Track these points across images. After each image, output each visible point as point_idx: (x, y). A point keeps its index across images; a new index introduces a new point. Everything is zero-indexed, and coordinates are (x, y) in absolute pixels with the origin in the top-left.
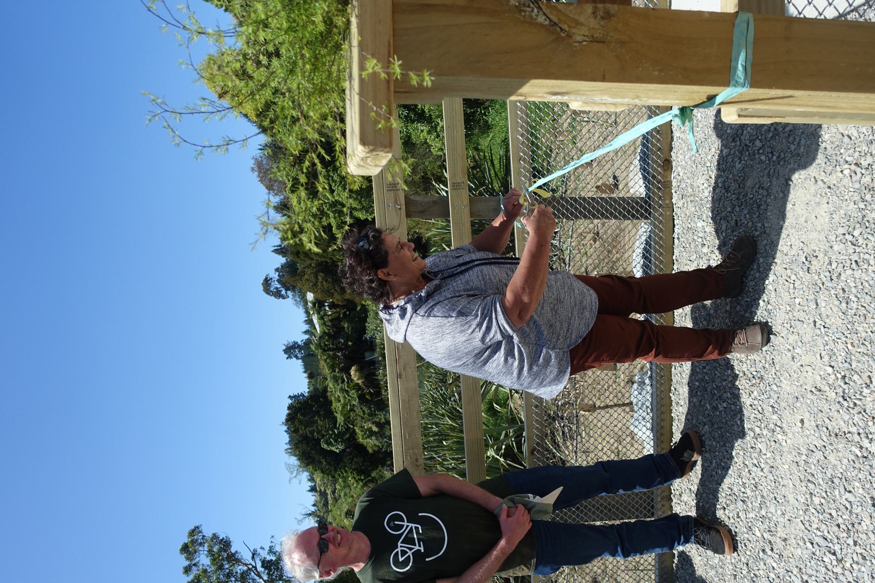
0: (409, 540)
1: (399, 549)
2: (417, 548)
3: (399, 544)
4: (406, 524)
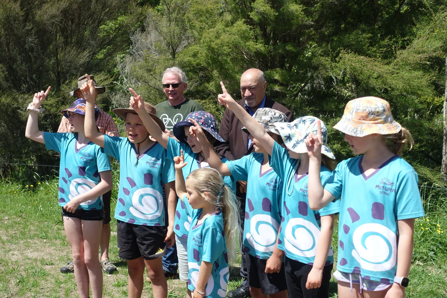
3: (170, 119)
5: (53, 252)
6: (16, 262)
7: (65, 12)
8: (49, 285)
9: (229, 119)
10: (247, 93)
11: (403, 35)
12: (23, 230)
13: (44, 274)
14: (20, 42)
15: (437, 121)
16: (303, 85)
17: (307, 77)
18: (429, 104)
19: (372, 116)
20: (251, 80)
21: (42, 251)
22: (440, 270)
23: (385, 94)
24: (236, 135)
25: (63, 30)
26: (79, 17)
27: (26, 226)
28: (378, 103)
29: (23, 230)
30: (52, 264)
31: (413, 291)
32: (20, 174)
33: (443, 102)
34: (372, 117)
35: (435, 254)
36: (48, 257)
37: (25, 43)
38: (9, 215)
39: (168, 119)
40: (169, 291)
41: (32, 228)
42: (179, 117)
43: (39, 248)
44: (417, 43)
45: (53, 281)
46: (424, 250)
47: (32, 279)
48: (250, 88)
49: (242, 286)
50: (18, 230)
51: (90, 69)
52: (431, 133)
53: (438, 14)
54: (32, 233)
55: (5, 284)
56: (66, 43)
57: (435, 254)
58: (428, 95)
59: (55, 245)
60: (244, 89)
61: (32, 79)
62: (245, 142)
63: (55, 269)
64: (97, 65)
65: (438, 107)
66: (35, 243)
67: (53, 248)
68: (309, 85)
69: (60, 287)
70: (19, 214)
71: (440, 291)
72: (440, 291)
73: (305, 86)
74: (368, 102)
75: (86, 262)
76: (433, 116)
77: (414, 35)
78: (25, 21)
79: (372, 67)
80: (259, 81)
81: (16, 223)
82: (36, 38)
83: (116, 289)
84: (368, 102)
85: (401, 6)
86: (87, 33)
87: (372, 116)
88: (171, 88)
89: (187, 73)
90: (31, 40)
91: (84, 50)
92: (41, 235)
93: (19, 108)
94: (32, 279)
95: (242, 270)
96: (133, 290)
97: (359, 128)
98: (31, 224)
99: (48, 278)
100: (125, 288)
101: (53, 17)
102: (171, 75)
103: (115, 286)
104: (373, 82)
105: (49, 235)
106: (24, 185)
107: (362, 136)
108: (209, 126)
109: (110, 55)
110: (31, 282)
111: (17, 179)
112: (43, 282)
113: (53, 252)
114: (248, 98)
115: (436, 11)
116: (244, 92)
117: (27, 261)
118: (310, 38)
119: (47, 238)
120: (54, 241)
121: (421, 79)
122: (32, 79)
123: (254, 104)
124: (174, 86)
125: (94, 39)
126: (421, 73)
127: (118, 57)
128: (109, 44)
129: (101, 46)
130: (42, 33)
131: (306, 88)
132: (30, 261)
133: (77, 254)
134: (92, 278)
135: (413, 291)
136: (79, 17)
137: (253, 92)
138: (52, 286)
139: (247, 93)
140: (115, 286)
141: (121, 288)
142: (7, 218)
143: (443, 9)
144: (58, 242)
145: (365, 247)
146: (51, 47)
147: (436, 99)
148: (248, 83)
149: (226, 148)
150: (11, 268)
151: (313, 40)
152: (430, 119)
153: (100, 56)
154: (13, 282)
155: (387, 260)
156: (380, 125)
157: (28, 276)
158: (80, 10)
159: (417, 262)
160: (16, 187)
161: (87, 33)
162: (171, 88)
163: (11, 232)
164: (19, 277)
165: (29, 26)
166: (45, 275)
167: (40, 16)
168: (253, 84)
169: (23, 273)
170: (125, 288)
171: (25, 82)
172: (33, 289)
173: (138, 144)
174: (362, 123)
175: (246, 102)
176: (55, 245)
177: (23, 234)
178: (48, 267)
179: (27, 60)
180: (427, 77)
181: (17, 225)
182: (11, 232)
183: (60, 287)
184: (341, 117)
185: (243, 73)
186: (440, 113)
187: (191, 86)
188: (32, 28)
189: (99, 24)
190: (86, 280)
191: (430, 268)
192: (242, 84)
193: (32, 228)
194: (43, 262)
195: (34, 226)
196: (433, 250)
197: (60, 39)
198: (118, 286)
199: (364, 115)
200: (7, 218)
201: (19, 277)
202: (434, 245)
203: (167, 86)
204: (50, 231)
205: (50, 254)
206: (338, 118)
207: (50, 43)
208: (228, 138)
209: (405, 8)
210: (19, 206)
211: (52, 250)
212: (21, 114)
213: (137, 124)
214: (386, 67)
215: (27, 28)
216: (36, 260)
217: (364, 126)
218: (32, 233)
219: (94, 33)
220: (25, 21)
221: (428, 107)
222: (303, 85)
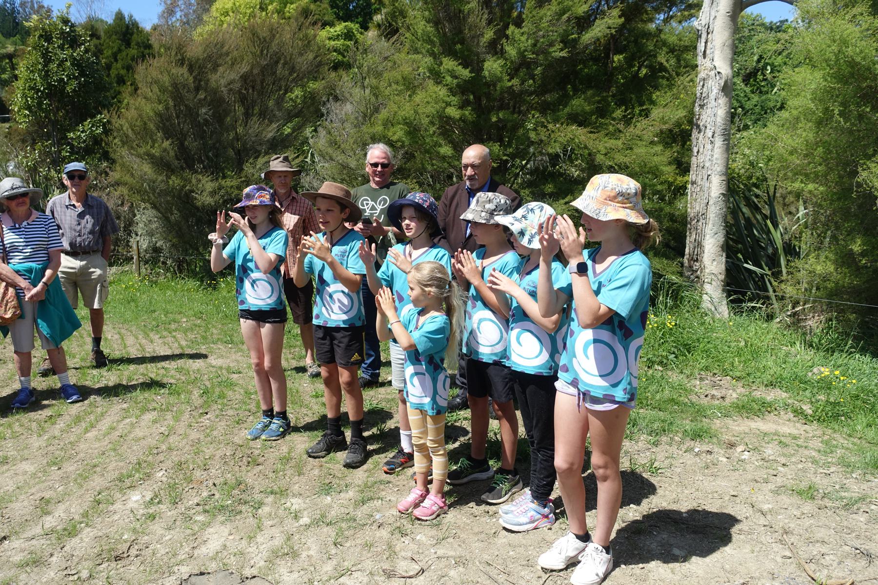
0: (373, 208)
1: (370, 202)
2: (368, 211)
4: (381, 207)
6: (198, 370)
7: (244, 78)
8: (237, 396)
10: (470, 172)
11: (641, 105)
12: (204, 334)
14: (191, 114)
15: (680, 205)
16: (524, 162)
17: (529, 153)
18: (670, 184)
19: (622, 198)
20: (475, 157)
21: (227, 358)
22: (682, 376)
24: (454, 220)
25: (243, 100)
26: (262, 83)
27: (207, 329)
28: (630, 185)
29: (204, 334)
30: (240, 373)
31: (651, 399)
32: (198, 269)
34: (620, 199)
35: (676, 357)
36: (235, 364)
37: (198, 115)
38: (187, 317)
39: (371, 203)
41: (215, 331)
43: (224, 354)
44: (656, 113)
45: (242, 391)
46: (664, 354)
47: (217, 390)
48: (473, 166)
49: (458, 396)
50: (198, 333)
51: (277, 145)
52: (672, 218)
54: (215, 337)
55: (188, 396)
56: (247, 115)
57: (676, 357)
58: (669, 172)
60: (466, 166)
61: (208, 157)
62: (464, 229)
63: (243, 378)
64: (283, 140)
65: (681, 188)
66: (219, 349)
67: (240, 354)
68: (532, 162)
70: (199, 315)
71: (682, 399)
72: (682, 399)
73: (526, 164)
74: (619, 180)
75: (266, 368)
76: (675, 198)
77: (653, 103)
78: (197, 89)
80: (484, 160)
81: (196, 326)
82: (210, 110)
83: (314, 400)
84: (619, 180)
85: (639, 69)
86: (271, 103)
87: (622, 198)
88: (379, 169)
91: (271, 122)
92: (225, 340)
93: (193, 191)
94: (217, 390)
95: (458, 376)
98: (213, 326)
99: (236, 388)
101: (231, 82)
102: (376, 153)
103: (312, 397)
105: (235, 339)
106: (202, 281)
107: (604, 220)
109: (298, 129)
112: (230, 393)
114: (471, 178)
116: (466, 170)
117: (211, 369)
118: (531, 107)
120: (240, 346)
122: (208, 157)
123: (477, 186)
124: (384, 166)
125: (280, 110)
127: (308, 131)
129: (289, 117)
130: (217, 102)
131: (529, 166)
132: (214, 370)
133: (256, 361)
134: (274, 386)
135: (651, 399)
136: (262, 83)
140: (312, 397)
141: (320, 399)
142: (185, 320)
145: (519, 343)
146: (229, 119)
147: (680, 179)
150: (193, 377)
151: (535, 109)
153: (287, 130)
154: (196, 393)
155: (537, 357)
156: (628, 210)
157: (213, 387)
158: (264, 75)
159: (656, 367)
160: (192, 284)
161: (271, 103)
162: (379, 169)
163: (191, 336)
165: (202, 95)
166: (231, 385)
167: (216, 81)
168: (477, 162)
169: (208, 383)
171: (201, 161)
172: (219, 401)
173: (331, 232)
174: (608, 205)
177: (204, 338)
178: (235, 376)
180: (668, 153)
182: (191, 336)
186: (684, 194)
187: (397, 163)
189: (286, 92)
190: (267, 389)
191: (670, 373)
193: (215, 331)
194: (228, 370)
196: (674, 353)
197: (239, 110)
198: (317, 397)
199: (613, 194)
200: (185, 320)
201: (202, 387)
202: (676, 347)
203: (375, 165)
204: (235, 335)
205: (238, 361)
207: (227, 115)
209: (644, 71)
210: (197, 307)
211: (238, 356)
212: (196, 199)
213: (329, 210)
215: (198, 97)
216: (221, 368)
217: (609, 209)
218: (215, 337)
219: (279, 102)
220: (197, 89)
221: (669, 188)
222: (524, 162)
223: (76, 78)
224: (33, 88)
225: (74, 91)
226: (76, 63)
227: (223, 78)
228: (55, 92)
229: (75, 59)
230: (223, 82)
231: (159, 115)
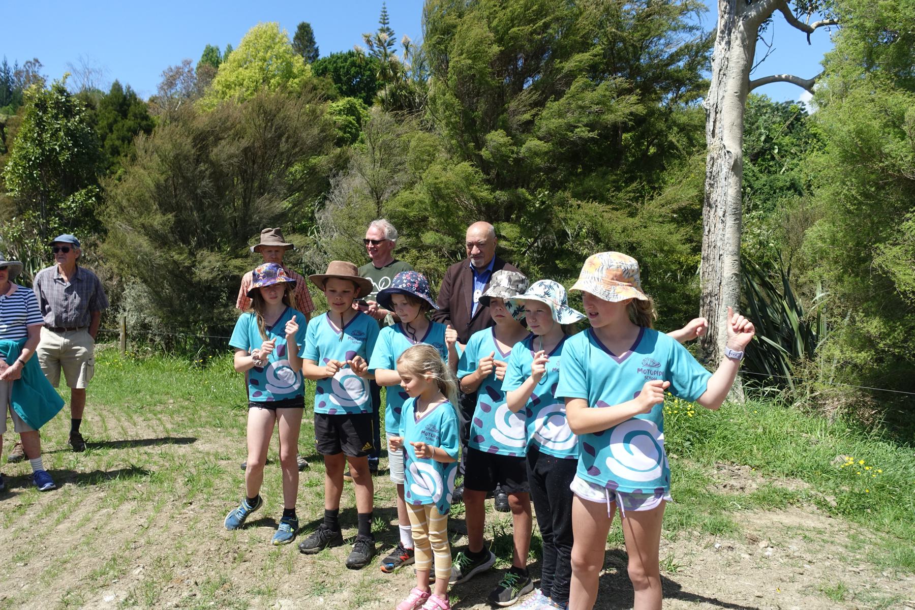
4: (382, 288)
5: (229, 443)
6: (184, 456)
7: (246, 150)
8: (225, 485)
9: (451, 282)
10: (475, 250)
12: (191, 416)
13: (219, 472)
19: (624, 277)
20: (480, 235)
21: (216, 443)
22: (699, 465)
23: (631, 250)
24: (458, 301)
25: (243, 173)
27: (195, 411)
29: (191, 416)
30: (229, 459)
33: (698, 262)
35: (691, 444)
36: (223, 449)
38: (174, 398)
40: (375, 491)
41: (203, 414)
42: (386, 281)
44: (669, 192)
45: (230, 479)
46: (679, 440)
48: (478, 244)
50: (185, 416)
53: (692, 158)
54: (203, 420)
55: (171, 484)
57: (691, 444)
59: (231, 435)
60: (471, 245)
65: (692, 267)
66: (207, 433)
69: (238, 488)
70: (187, 396)
71: (699, 489)
79: (616, 222)
80: (488, 236)
81: (183, 407)
83: (308, 490)
89: (399, 227)
90: (206, 184)
92: (214, 423)
94: (203, 478)
96: (331, 491)
97: (612, 291)
98: (202, 408)
100: (318, 489)
101: (231, 157)
102: (378, 229)
104: (616, 238)
105: (225, 423)
107: (616, 301)
108: (423, 292)
110: (203, 481)
111: (183, 353)
112: (217, 481)
113: (229, 443)
114: (476, 257)
115: (690, 154)
117: (198, 454)
119: (221, 426)
120: (230, 430)
121: (676, 237)
126: (673, 226)
128: (298, 190)
130: (218, 175)
132: (201, 455)
137: (483, 249)
138: (229, 486)
139: (475, 250)
141: (314, 488)
142: (172, 401)
143: (698, 151)
144: (235, 431)
148: (477, 239)
149: (445, 316)
150: (178, 464)
152: (684, 282)
154: (180, 481)
157: (199, 474)
160: (182, 363)
164: (187, 474)
165: (202, 167)
166: (219, 472)
168: (483, 240)
169: (193, 470)
170: (318, 489)
172: (205, 490)
175: (473, 261)
176: (231, 435)
177: (192, 421)
178: (224, 463)
179: (200, 208)
181: (185, 411)
183: (238, 488)
184: (577, 277)
185: (469, 226)
188: (206, 170)
192: (469, 239)
193: (203, 414)
194: (217, 456)
195: (205, 411)
196: (689, 440)
198: (311, 486)
200: (172, 401)
201: (187, 474)
202: (690, 433)
204: (225, 418)
205: (226, 446)
206: (573, 280)
208: (449, 304)
209: (652, 150)
211: (227, 441)
213: (345, 292)
214: (631, 220)
216: (208, 454)
217: (618, 289)
218: (203, 420)
220: (198, 161)
223: (69, 149)
224: (25, 157)
225: (67, 161)
226: (70, 133)
227: (225, 151)
228: (48, 161)
229: (69, 129)
230: (224, 156)
231: (158, 186)
